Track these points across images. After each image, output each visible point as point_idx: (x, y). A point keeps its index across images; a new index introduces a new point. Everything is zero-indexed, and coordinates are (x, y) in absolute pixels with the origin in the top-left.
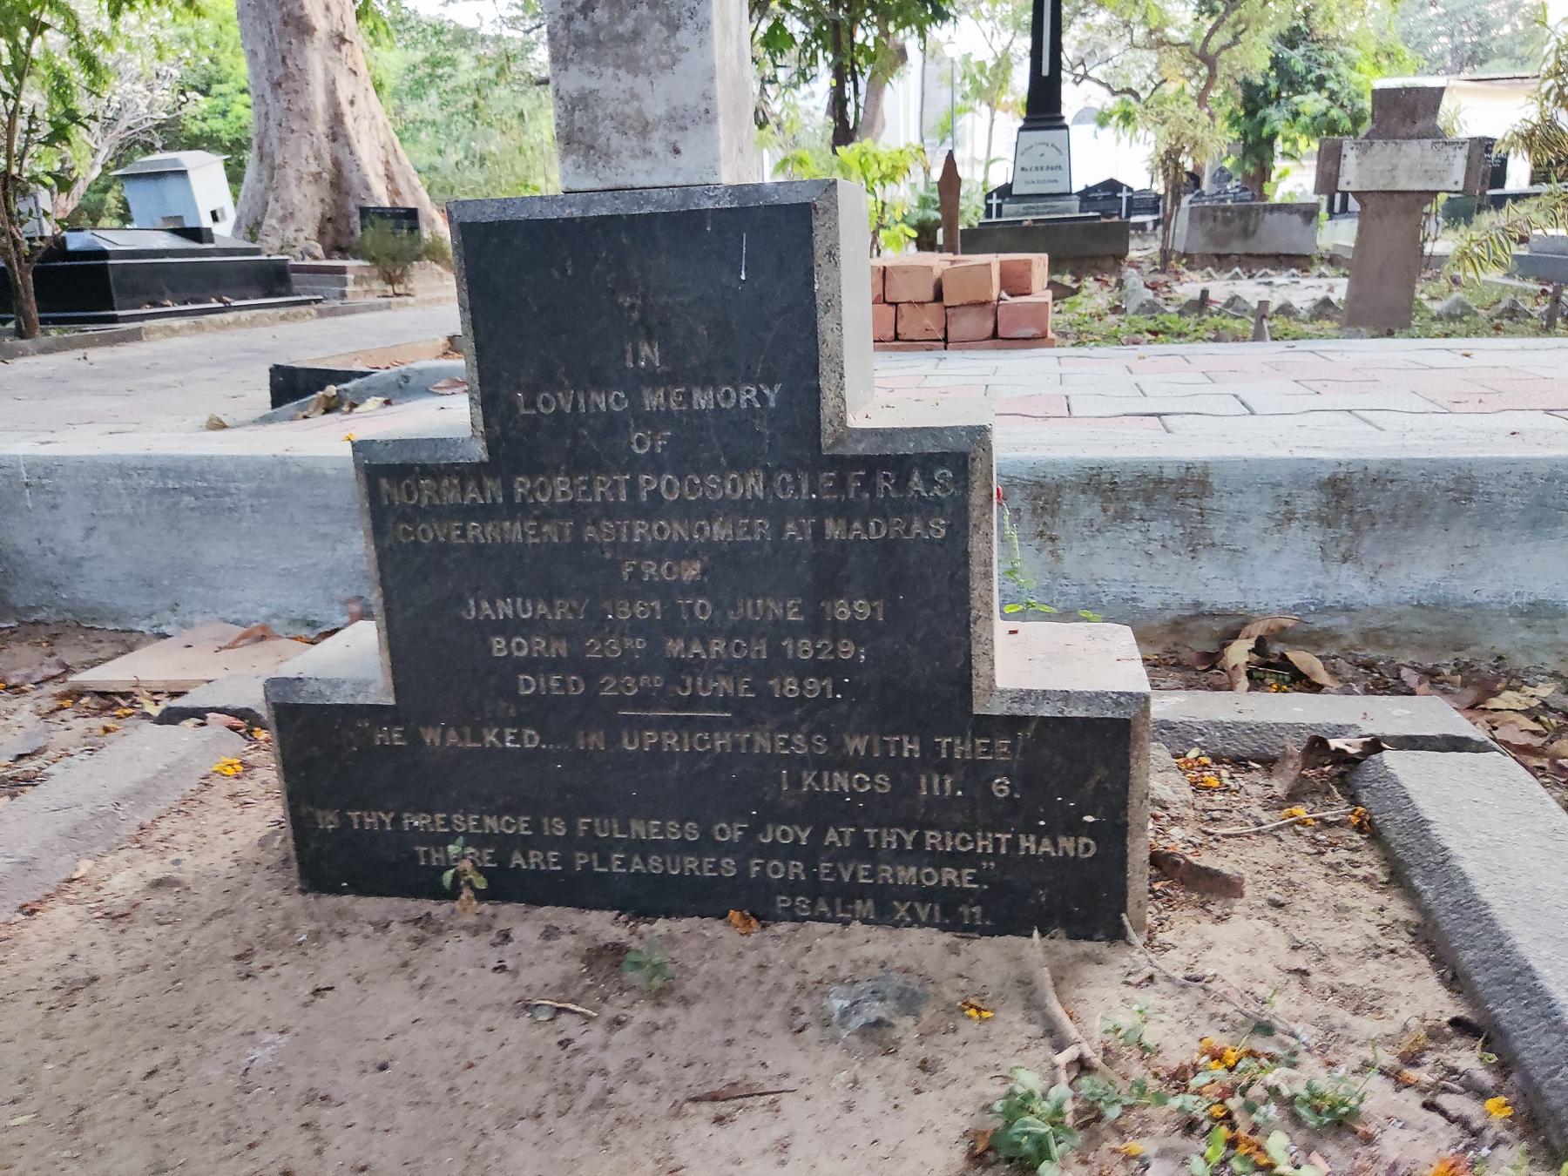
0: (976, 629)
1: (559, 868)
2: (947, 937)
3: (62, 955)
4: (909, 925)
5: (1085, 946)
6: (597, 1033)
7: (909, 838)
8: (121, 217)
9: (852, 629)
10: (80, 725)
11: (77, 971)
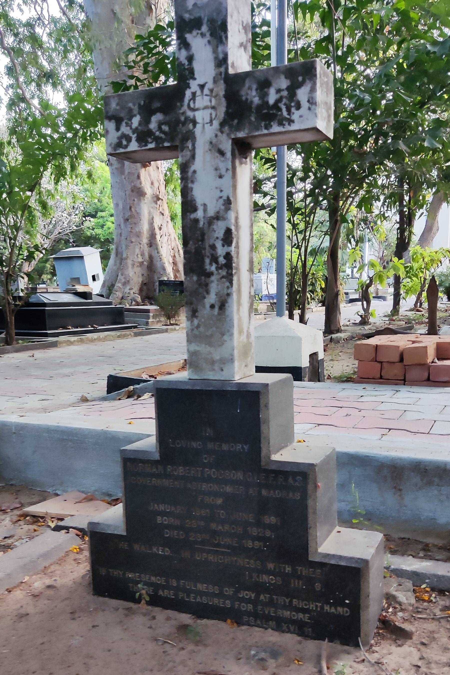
0: (310, 531)
1: (173, 597)
2: (299, 638)
3: (18, 606)
4: (287, 632)
5: (346, 648)
6: (175, 650)
7: (287, 601)
8: (51, 273)
9: (270, 527)
10: (26, 527)
11: (23, 611)
